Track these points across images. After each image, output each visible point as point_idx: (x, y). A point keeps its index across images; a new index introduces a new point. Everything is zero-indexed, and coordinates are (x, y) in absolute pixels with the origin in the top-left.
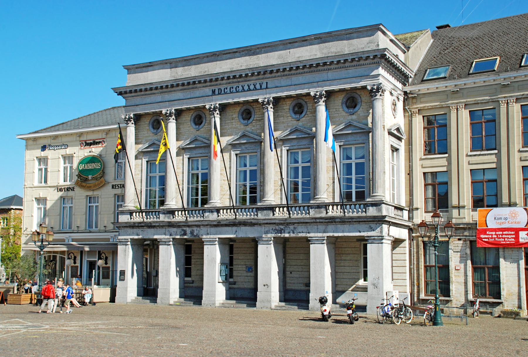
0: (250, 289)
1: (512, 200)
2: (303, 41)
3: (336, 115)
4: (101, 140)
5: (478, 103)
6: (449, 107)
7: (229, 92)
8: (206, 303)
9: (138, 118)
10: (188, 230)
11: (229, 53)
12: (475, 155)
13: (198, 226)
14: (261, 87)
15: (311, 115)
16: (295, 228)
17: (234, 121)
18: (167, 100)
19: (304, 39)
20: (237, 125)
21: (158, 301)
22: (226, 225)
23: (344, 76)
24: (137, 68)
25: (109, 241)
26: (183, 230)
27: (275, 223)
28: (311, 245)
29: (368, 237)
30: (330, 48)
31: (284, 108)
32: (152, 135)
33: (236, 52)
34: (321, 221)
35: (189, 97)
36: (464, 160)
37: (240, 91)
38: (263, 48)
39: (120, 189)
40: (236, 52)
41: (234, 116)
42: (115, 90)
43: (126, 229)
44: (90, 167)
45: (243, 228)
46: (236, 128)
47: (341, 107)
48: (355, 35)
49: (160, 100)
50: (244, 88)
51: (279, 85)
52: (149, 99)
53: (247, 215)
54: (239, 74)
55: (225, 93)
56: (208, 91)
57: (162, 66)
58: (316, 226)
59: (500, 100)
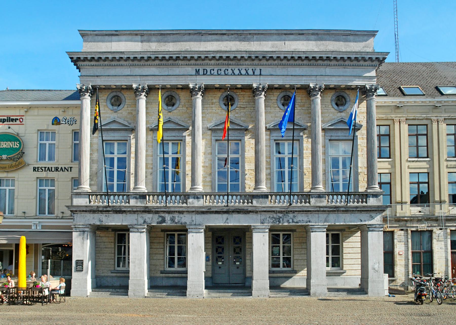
1: (442, 199)
2: (300, 34)
3: (325, 111)
4: (18, 118)
5: (415, 119)
6: (393, 120)
7: (216, 73)
8: (192, 293)
9: (95, 91)
10: (168, 217)
11: (216, 34)
12: (413, 161)
13: (180, 212)
14: (254, 73)
16: (294, 216)
17: (213, 106)
18: (137, 74)
19: (301, 32)
20: (217, 111)
21: (129, 293)
22: (217, 212)
23: (342, 74)
24: (96, 35)
25: (31, 228)
26: (160, 216)
27: (274, 211)
28: (370, 233)
29: (370, 225)
30: (327, 46)
31: (271, 98)
32: (109, 111)
33: (225, 34)
34: (325, 209)
35: (167, 74)
36: (405, 165)
37: (230, 74)
38: (256, 34)
40: (225, 34)
41: (214, 101)
43: (83, 214)
44: (5, 146)
45: (236, 216)
46: (217, 113)
47: (330, 104)
48: (351, 38)
49: (129, 73)
50: (235, 72)
51: (274, 73)
52: (112, 71)
53: (240, 202)
54: (234, 55)
55: (211, 74)
56: (191, 70)
57: (130, 37)
58: (317, 215)
59: (432, 118)
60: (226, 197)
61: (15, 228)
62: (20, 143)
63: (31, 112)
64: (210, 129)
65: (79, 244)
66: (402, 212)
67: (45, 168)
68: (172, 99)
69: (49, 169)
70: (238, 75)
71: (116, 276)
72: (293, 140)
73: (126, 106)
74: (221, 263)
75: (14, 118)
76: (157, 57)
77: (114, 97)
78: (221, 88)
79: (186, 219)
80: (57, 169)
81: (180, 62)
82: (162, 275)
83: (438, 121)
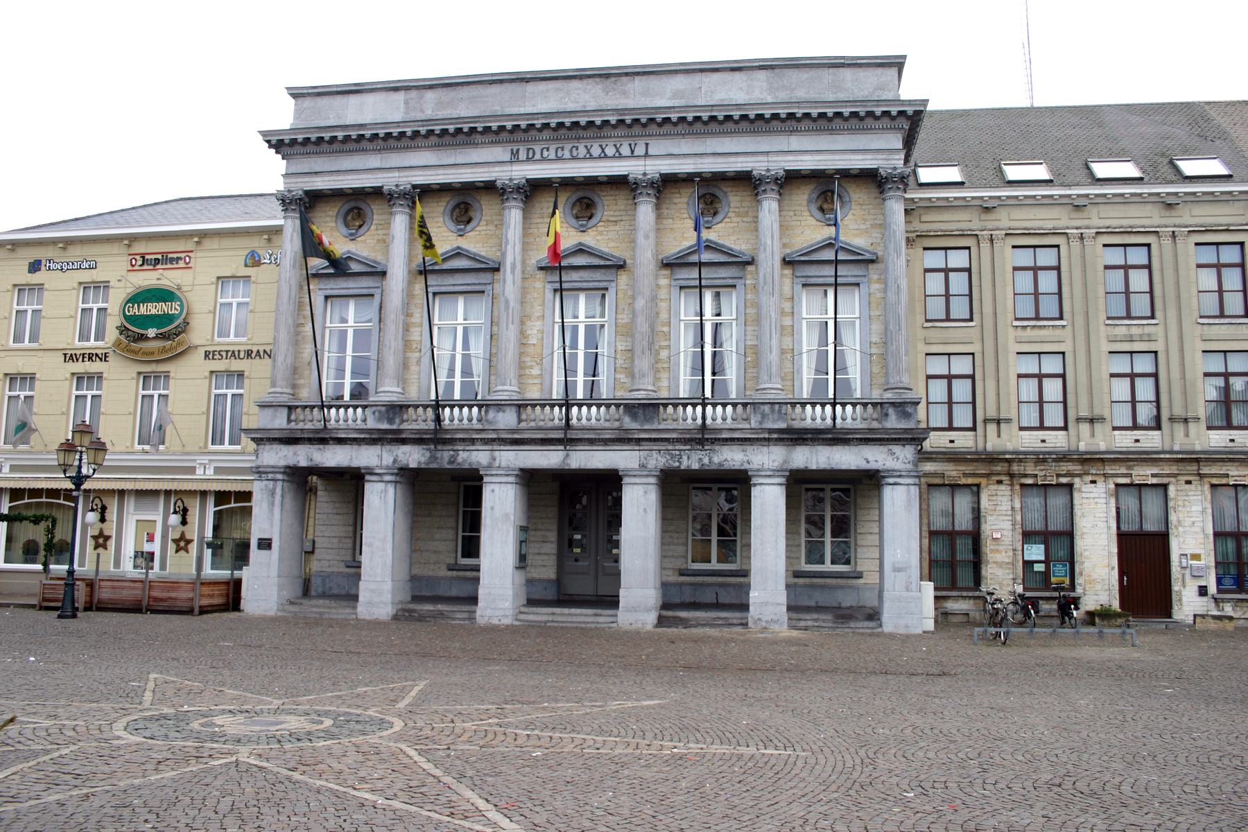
0: (549, 581)
4: (182, 255)
7: (553, 156)
14: (632, 152)
15: (739, 219)
27: (667, 440)
37: (581, 156)
39: (224, 361)
42: (264, 134)
44: (154, 311)
50: (592, 151)
56: (500, 153)
60: (699, 408)
61: (129, 473)
62: (181, 306)
63: (207, 243)
64: (541, 268)
65: (265, 505)
66: (1186, 441)
67: (227, 352)
68: (466, 211)
69: (234, 355)
70: (614, 157)
71: (805, 586)
72: (701, 287)
73: (373, 227)
74: (578, 550)
75: (175, 256)
76: (533, 125)
77: (351, 210)
78: (567, 183)
79: (477, 457)
80: (249, 354)
81: (479, 138)
82: (450, 573)
83: (992, 240)
